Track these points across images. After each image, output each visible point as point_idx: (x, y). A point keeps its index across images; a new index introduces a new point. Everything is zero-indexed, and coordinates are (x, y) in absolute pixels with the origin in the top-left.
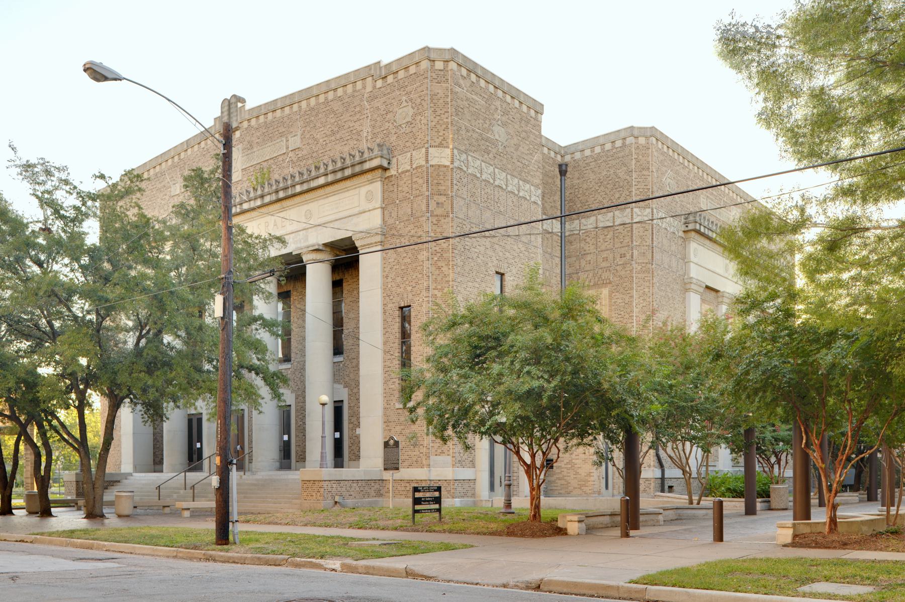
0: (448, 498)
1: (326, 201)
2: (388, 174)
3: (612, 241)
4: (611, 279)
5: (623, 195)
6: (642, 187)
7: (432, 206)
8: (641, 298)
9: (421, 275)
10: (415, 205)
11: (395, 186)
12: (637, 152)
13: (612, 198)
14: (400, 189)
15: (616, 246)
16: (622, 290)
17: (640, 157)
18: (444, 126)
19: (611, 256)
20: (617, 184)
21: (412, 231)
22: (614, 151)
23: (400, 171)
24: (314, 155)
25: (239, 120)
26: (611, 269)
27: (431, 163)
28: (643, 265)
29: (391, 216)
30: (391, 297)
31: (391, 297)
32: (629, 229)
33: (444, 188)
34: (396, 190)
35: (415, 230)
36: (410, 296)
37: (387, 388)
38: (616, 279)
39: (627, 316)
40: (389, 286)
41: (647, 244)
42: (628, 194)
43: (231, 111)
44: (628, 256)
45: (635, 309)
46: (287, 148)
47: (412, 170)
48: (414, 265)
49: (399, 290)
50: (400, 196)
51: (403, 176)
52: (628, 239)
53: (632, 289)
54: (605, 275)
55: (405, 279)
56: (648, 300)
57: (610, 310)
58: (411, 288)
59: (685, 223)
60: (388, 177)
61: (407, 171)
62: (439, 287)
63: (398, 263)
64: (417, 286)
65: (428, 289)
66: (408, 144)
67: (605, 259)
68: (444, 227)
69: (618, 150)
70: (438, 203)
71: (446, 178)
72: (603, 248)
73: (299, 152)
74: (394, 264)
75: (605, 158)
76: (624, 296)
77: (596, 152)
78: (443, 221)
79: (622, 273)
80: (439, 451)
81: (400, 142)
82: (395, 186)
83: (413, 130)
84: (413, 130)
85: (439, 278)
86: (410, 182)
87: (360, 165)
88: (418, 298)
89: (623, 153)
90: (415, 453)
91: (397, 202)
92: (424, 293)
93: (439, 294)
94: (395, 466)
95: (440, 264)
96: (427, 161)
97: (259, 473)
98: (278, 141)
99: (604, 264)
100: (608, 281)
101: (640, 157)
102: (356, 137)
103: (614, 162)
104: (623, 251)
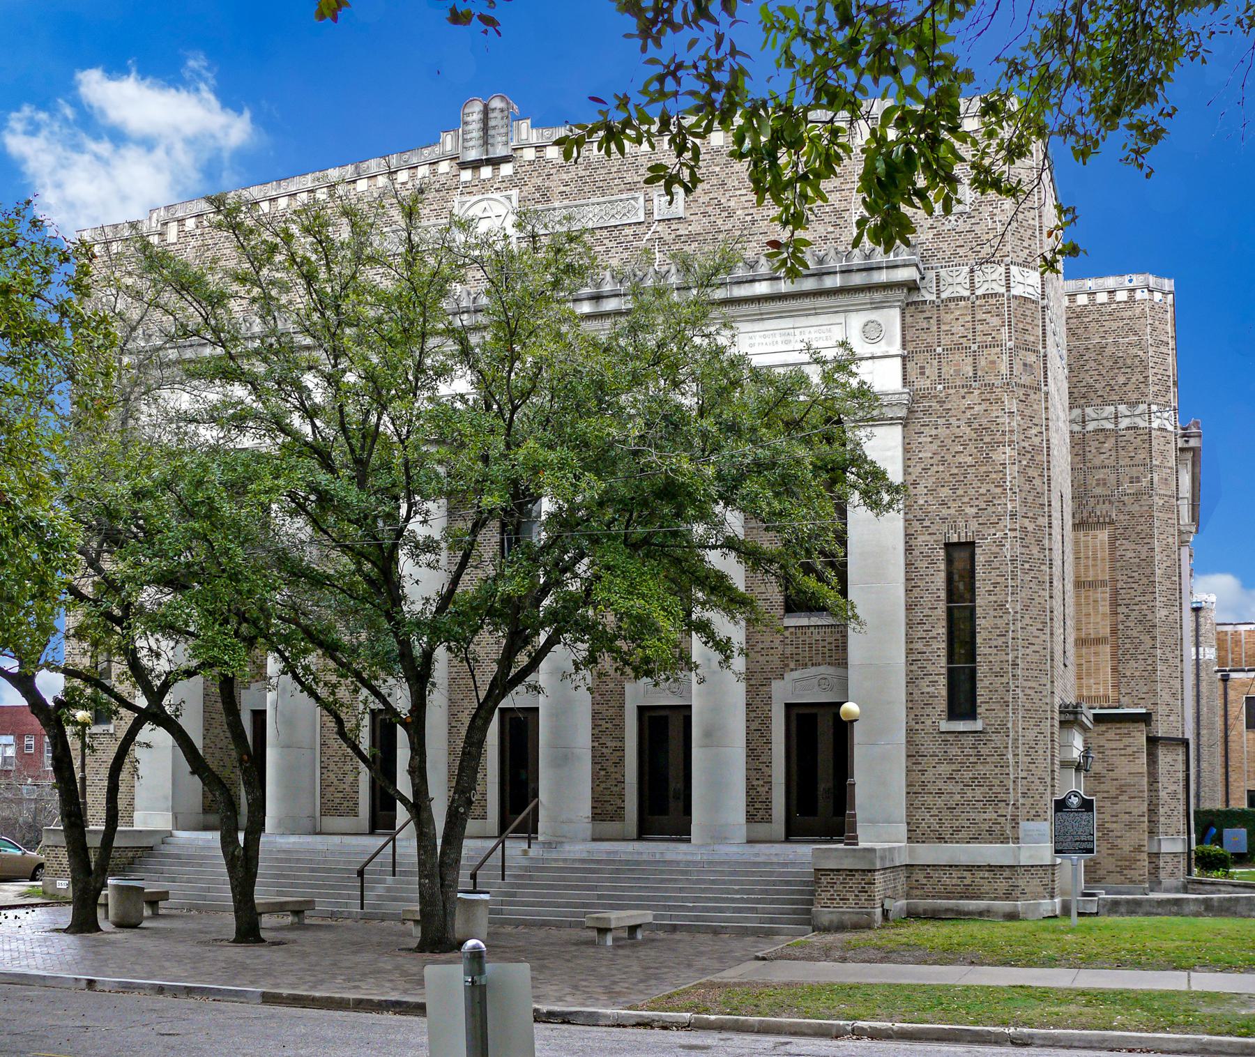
0: (1044, 897)
1: (757, 326)
2: (915, 298)
3: (1113, 453)
4: (1114, 517)
5: (1133, 380)
6: (1161, 371)
7: (1017, 368)
8: (1165, 553)
9: (999, 490)
10: (983, 362)
11: (933, 321)
12: (1153, 314)
13: (1113, 382)
14: (944, 327)
15: (1122, 463)
16: (1134, 536)
17: (1157, 322)
18: (1030, 232)
19: (1113, 478)
20: (1121, 361)
21: (977, 408)
22: (1114, 306)
23: (944, 296)
24: (721, 237)
25: (514, 144)
26: (1112, 499)
27: (1014, 292)
28: (1166, 499)
29: (923, 373)
30: (927, 523)
31: (927, 523)
32: (1146, 437)
33: (1032, 339)
34: (935, 328)
35: (984, 406)
36: (974, 525)
37: (916, 692)
38: (1122, 517)
39: (1145, 581)
40: (921, 502)
41: (1170, 465)
42: (1143, 380)
43: (492, 123)
44: (1145, 482)
45: (1158, 572)
46: (649, 213)
47: (973, 298)
48: (984, 469)
49: (945, 512)
50: (945, 340)
51: (952, 305)
52: (1142, 455)
53: (1152, 537)
54: (1101, 509)
55: (960, 492)
56: (1173, 557)
57: (1113, 569)
58: (974, 510)
59: (1184, 436)
60: (915, 302)
61: (962, 298)
62: (1031, 515)
63: (943, 461)
64: (990, 509)
65: (1013, 515)
66: (961, 251)
67: (1102, 483)
68: (1035, 407)
69: (1122, 305)
70: (1025, 365)
71: (1035, 322)
72: (1097, 462)
73: (680, 226)
74: (931, 461)
75: (1096, 316)
76: (1138, 548)
77: (1079, 303)
78: (1032, 396)
79: (1136, 508)
80: (1033, 812)
81: (944, 246)
82: (933, 321)
83: (975, 228)
84: (975, 228)
85: (1030, 499)
86: (969, 318)
87: (864, 274)
88: (993, 531)
89: (1130, 313)
90: (985, 816)
91: (939, 350)
92: (1007, 521)
93: (1031, 527)
94: (1089, 846)
95: (1031, 472)
96: (1008, 288)
97: (567, 847)
98: (624, 196)
99: (1099, 491)
100: (1107, 520)
101: (1157, 322)
102: (833, 219)
103: (1114, 325)
104: (1134, 472)
